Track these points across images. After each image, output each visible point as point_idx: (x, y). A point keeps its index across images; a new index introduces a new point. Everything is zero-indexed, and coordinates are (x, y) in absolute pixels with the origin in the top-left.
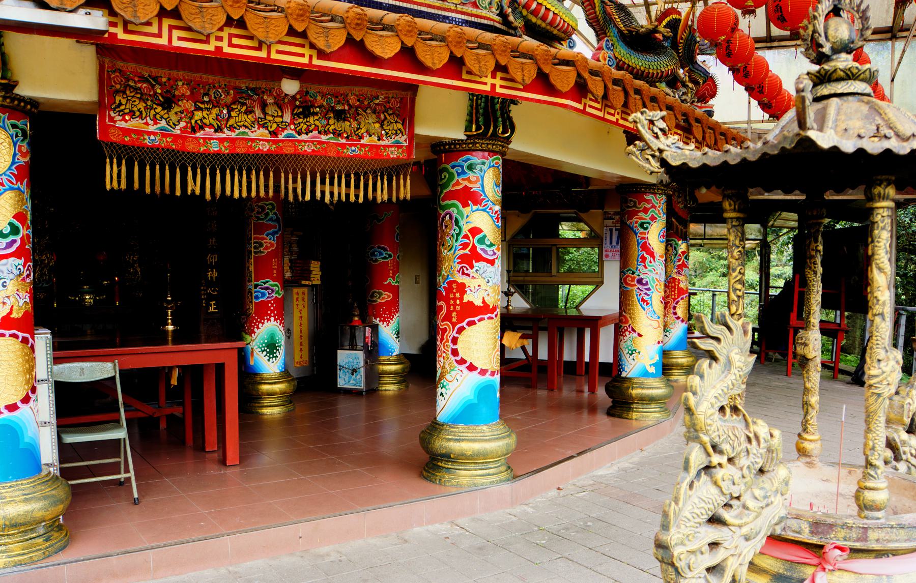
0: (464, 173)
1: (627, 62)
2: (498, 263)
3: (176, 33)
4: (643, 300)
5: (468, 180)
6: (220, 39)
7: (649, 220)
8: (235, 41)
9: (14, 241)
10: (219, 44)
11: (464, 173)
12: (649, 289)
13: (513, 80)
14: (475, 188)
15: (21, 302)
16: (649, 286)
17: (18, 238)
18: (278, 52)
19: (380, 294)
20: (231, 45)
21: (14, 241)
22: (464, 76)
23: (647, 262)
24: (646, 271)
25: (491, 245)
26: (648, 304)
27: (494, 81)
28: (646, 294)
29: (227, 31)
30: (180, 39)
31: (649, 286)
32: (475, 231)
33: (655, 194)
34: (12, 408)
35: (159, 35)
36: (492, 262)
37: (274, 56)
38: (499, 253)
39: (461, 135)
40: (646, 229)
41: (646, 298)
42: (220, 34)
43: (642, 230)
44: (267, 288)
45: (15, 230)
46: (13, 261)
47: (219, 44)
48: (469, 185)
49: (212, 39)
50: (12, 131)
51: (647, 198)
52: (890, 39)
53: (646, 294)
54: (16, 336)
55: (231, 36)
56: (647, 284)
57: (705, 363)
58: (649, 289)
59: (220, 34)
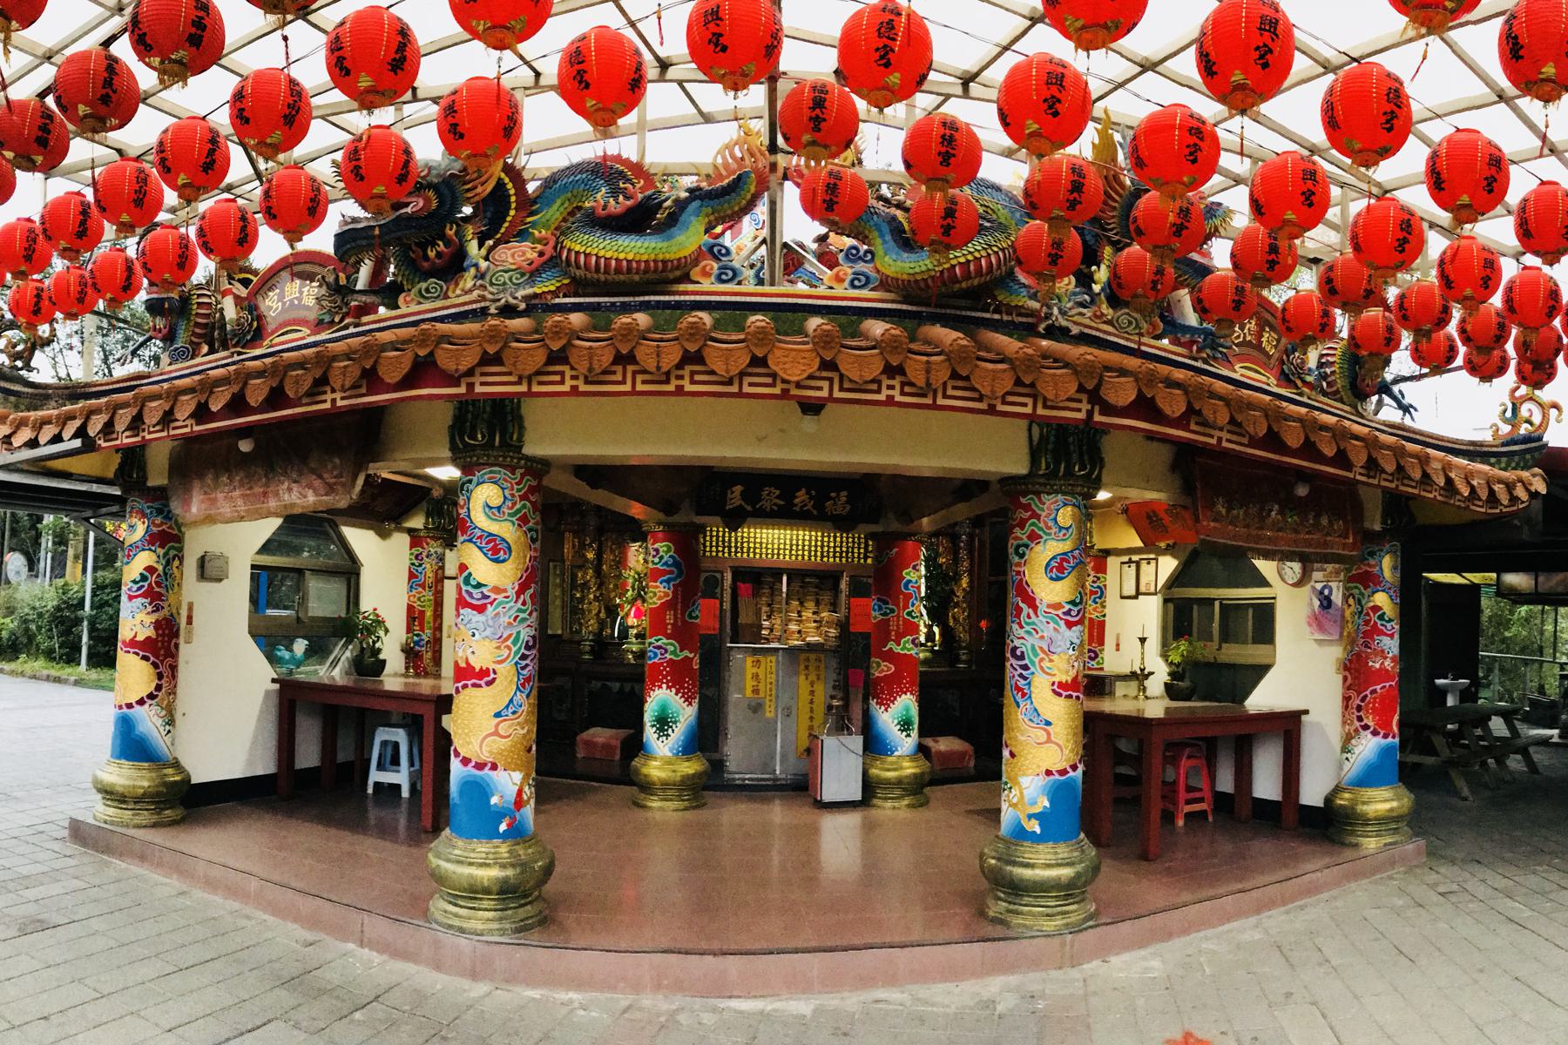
2: (1397, 636)
3: (639, 378)
4: (1019, 689)
7: (1026, 541)
12: (1026, 668)
16: (1027, 661)
18: (751, 385)
19: (879, 665)
20: (693, 382)
22: (1193, 427)
23: (1024, 614)
24: (1021, 633)
25: (1390, 620)
26: (1024, 695)
28: (1021, 675)
29: (688, 368)
30: (644, 382)
31: (1027, 661)
32: (1376, 609)
33: (1038, 494)
35: (623, 382)
36: (1392, 636)
38: (1397, 627)
39: (1021, 468)
40: (1022, 556)
41: (1022, 683)
43: (1017, 559)
44: (659, 647)
46: (140, 600)
51: (1023, 500)
53: (1021, 675)
55: (693, 373)
56: (1022, 657)
57: (550, 887)
58: (1026, 668)
59: (680, 372)
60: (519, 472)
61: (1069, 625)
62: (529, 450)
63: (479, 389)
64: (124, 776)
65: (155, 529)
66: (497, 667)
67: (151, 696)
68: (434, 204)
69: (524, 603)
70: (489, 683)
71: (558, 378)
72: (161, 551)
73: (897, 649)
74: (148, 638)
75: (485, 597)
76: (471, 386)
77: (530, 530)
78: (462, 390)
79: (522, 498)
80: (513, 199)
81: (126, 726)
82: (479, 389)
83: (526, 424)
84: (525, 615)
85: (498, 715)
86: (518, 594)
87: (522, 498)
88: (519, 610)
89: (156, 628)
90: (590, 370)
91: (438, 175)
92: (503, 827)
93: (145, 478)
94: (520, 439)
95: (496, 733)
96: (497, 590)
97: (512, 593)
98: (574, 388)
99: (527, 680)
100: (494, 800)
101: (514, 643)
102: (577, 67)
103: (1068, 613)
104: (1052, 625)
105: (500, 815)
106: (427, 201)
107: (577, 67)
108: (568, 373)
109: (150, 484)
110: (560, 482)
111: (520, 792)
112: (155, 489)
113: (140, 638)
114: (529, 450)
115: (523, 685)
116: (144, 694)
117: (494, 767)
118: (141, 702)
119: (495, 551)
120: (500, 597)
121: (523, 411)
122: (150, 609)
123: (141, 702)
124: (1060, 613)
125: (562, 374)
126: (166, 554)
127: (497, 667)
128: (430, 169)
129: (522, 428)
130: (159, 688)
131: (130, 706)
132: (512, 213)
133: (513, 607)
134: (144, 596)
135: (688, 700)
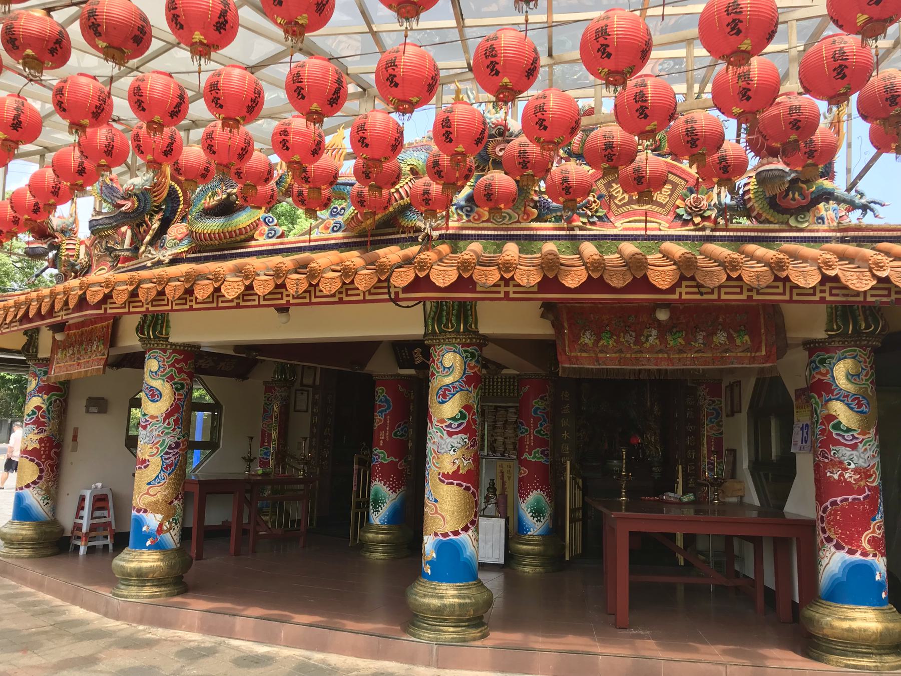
0: (817, 367)
1: (230, 229)
5: (820, 373)
6: (823, 291)
8: (834, 292)
9: (462, 423)
10: (823, 295)
11: (817, 367)
13: (519, 285)
14: (827, 379)
15: (466, 462)
17: (465, 421)
18: (726, 293)
20: (831, 295)
21: (462, 423)
27: (507, 289)
34: (456, 533)
35: (784, 294)
37: (723, 297)
42: (823, 288)
45: (463, 416)
47: (823, 295)
48: (822, 378)
49: (893, 293)
50: (464, 355)
52: (469, 64)
54: (460, 485)
55: (831, 288)
60: (168, 352)
61: (450, 434)
62: (172, 340)
63: (109, 311)
64: (25, 530)
65: (42, 384)
66: (150, 458)
67: (34, 483)
68: (136, 204)
69: (169, 424)
70: (145, 467)
71: (280, 296)
72: (45, 397)
73: (530, 458)
74: (35, 449)
75: (147, 421)
76: (106, 309)
77: (175, 384)
78: (102, 311)
79: (172, 365)
80: (181, 199)
81: (19, 499)
82: (109, 311)
83: (171, 324)
84: (170, 431)
85: (149, 484)
86: (165, 420)
87: (172, 365)
88: (165, 428)
89: (40, 443)
90: (297, 292)
91: (139, 189)
92: (148, 543)
93: (37, 352)
94: (167, 334)
95: (148, 493)
96: (152, 417)
97: (161, 419)
98: (238, 304)
99: (170, 465)
100: (144, 529)
101: (161, 446)
102: (491, 59)
103: (450, 426)
104: (439, 434)
105: (148, 536)
106: (133, 203)
107: (491, 59)
108: (285, 293)
109: (39, 356)
110: (490, 352)
111: (161, 525)
112: (43, 360)
113: (30, 448)
114: (172, 340)
115: (166, 468)
116: (30, 482)
117: (145, 511)
118: (28, 486)
119: (153, 396)
120: (154, 421)
121: (170, 318)
122: (36, 431)
123: (28, 486)
124: (443, 425)
125: (282, 293)
126: (48, 399)
127: (150, 458)
128: (134, 186)
129: (168, 327)
130: (40, 478)
131: (21, 488)
132: (181, 207)
133: (161, 426)
134: (32, 423)
135: (393, 489)
